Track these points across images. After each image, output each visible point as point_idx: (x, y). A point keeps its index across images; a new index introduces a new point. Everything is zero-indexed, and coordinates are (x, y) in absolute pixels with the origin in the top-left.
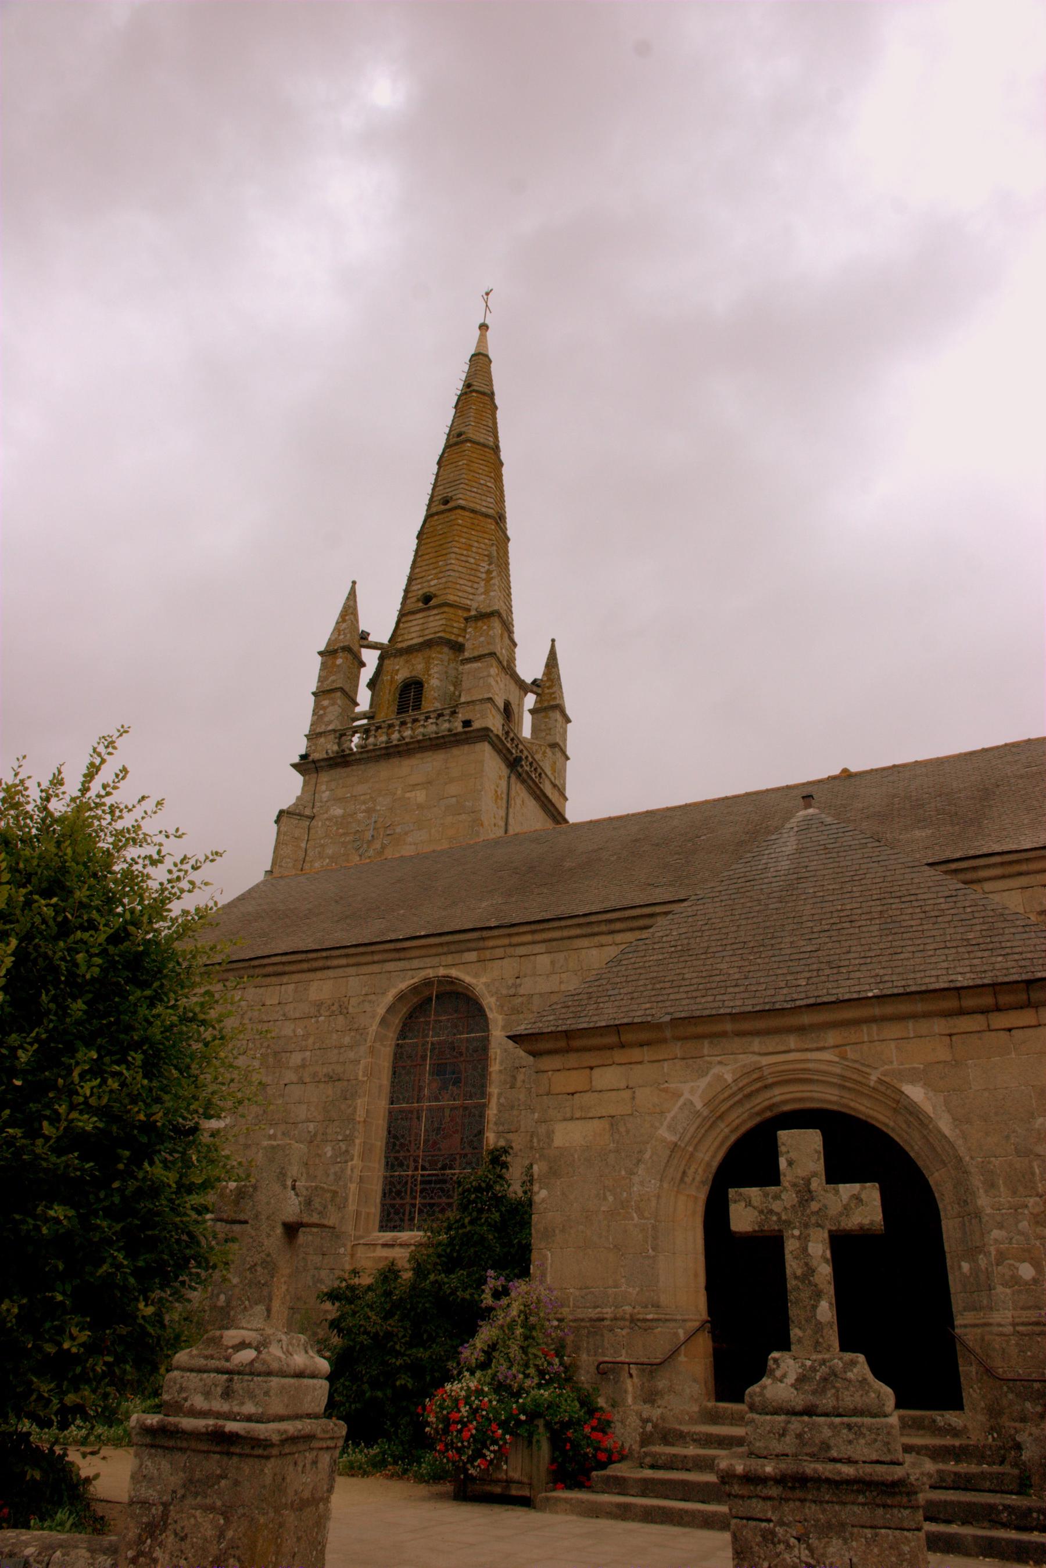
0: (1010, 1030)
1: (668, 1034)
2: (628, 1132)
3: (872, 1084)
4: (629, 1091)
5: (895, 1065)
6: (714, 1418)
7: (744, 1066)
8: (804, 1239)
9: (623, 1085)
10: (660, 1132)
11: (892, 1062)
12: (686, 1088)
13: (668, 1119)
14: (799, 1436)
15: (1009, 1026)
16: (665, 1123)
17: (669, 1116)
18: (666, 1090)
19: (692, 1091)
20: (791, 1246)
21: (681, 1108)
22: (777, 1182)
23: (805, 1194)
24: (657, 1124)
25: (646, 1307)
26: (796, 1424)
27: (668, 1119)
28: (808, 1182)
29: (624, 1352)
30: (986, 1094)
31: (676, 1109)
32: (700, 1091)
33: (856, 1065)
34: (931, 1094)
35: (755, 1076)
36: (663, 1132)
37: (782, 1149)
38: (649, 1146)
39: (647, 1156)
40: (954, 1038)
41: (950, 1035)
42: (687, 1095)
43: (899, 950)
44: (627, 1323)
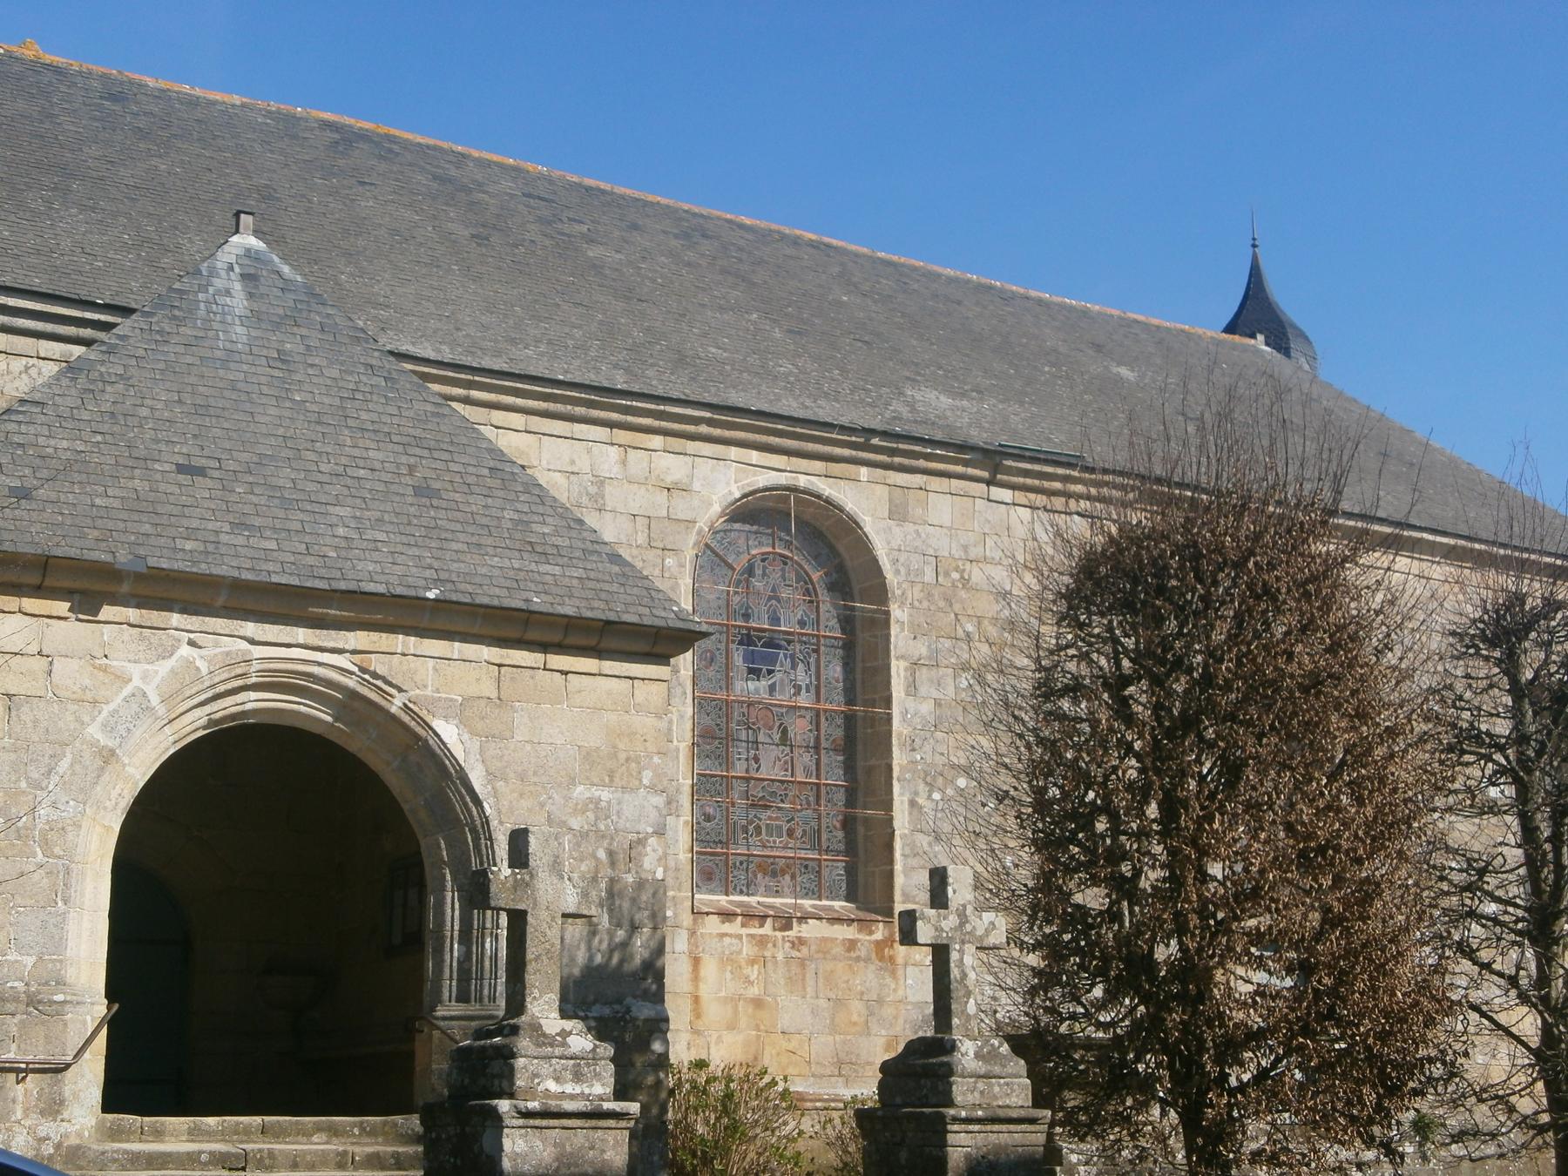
0: (566, 673)
1: (125, 588)
2: (36, 722)
3: (393, 710)
4: (45, 661)
5: (429, 692)
6: (115, 1134)
7: (228, 654)
8: (961, 952)
9: (34, 649)
10: (90, 730)
11: (425, 686)
12: (135, 671)
13: (105, 713)
14: (982, 1092)
15: (566, 668)
16: (100, 719)
17: (106, 709)
18: (104, 669)
19: (145, 677)
20: (954, 956)
21: (125, 700)
22: (946, 907)
23: (962, 915)
24: (86, 719)
25: (47, 984)
26: (981, 1085)
27: (105, 713)
28: (964, 906)
29: (14, 1047)
30: (528, 747)
31: (119, 700)
32: (157, 680)
33: (379, 683)
34: (466, 737)
35: (239, 671)
36: (94, 731)
37: (950, 880)
38: (68, 750)
39: (64, 765)
40: (503, 669)
41: (500, 666)
42: (136, 682)
43: (449, 536)
44: (22, 1007)
